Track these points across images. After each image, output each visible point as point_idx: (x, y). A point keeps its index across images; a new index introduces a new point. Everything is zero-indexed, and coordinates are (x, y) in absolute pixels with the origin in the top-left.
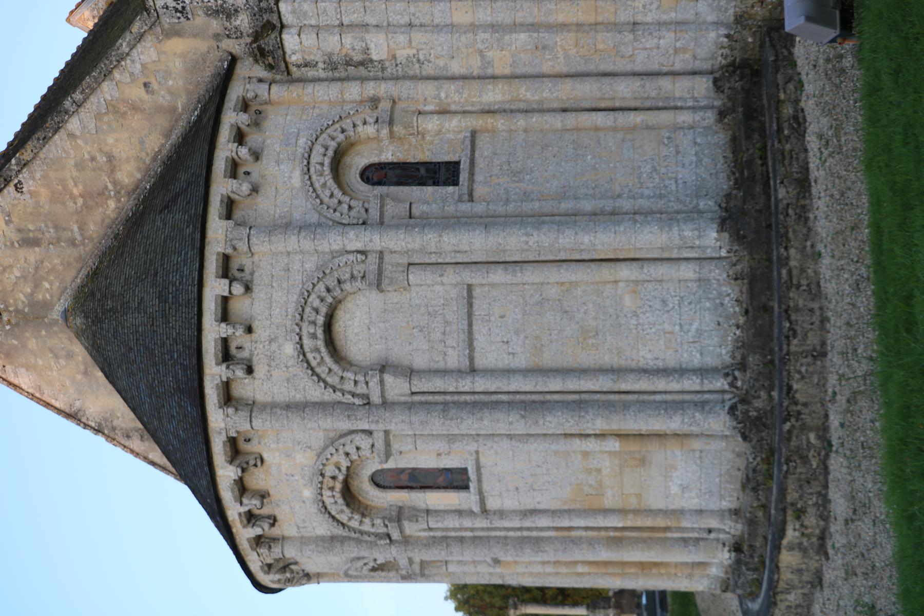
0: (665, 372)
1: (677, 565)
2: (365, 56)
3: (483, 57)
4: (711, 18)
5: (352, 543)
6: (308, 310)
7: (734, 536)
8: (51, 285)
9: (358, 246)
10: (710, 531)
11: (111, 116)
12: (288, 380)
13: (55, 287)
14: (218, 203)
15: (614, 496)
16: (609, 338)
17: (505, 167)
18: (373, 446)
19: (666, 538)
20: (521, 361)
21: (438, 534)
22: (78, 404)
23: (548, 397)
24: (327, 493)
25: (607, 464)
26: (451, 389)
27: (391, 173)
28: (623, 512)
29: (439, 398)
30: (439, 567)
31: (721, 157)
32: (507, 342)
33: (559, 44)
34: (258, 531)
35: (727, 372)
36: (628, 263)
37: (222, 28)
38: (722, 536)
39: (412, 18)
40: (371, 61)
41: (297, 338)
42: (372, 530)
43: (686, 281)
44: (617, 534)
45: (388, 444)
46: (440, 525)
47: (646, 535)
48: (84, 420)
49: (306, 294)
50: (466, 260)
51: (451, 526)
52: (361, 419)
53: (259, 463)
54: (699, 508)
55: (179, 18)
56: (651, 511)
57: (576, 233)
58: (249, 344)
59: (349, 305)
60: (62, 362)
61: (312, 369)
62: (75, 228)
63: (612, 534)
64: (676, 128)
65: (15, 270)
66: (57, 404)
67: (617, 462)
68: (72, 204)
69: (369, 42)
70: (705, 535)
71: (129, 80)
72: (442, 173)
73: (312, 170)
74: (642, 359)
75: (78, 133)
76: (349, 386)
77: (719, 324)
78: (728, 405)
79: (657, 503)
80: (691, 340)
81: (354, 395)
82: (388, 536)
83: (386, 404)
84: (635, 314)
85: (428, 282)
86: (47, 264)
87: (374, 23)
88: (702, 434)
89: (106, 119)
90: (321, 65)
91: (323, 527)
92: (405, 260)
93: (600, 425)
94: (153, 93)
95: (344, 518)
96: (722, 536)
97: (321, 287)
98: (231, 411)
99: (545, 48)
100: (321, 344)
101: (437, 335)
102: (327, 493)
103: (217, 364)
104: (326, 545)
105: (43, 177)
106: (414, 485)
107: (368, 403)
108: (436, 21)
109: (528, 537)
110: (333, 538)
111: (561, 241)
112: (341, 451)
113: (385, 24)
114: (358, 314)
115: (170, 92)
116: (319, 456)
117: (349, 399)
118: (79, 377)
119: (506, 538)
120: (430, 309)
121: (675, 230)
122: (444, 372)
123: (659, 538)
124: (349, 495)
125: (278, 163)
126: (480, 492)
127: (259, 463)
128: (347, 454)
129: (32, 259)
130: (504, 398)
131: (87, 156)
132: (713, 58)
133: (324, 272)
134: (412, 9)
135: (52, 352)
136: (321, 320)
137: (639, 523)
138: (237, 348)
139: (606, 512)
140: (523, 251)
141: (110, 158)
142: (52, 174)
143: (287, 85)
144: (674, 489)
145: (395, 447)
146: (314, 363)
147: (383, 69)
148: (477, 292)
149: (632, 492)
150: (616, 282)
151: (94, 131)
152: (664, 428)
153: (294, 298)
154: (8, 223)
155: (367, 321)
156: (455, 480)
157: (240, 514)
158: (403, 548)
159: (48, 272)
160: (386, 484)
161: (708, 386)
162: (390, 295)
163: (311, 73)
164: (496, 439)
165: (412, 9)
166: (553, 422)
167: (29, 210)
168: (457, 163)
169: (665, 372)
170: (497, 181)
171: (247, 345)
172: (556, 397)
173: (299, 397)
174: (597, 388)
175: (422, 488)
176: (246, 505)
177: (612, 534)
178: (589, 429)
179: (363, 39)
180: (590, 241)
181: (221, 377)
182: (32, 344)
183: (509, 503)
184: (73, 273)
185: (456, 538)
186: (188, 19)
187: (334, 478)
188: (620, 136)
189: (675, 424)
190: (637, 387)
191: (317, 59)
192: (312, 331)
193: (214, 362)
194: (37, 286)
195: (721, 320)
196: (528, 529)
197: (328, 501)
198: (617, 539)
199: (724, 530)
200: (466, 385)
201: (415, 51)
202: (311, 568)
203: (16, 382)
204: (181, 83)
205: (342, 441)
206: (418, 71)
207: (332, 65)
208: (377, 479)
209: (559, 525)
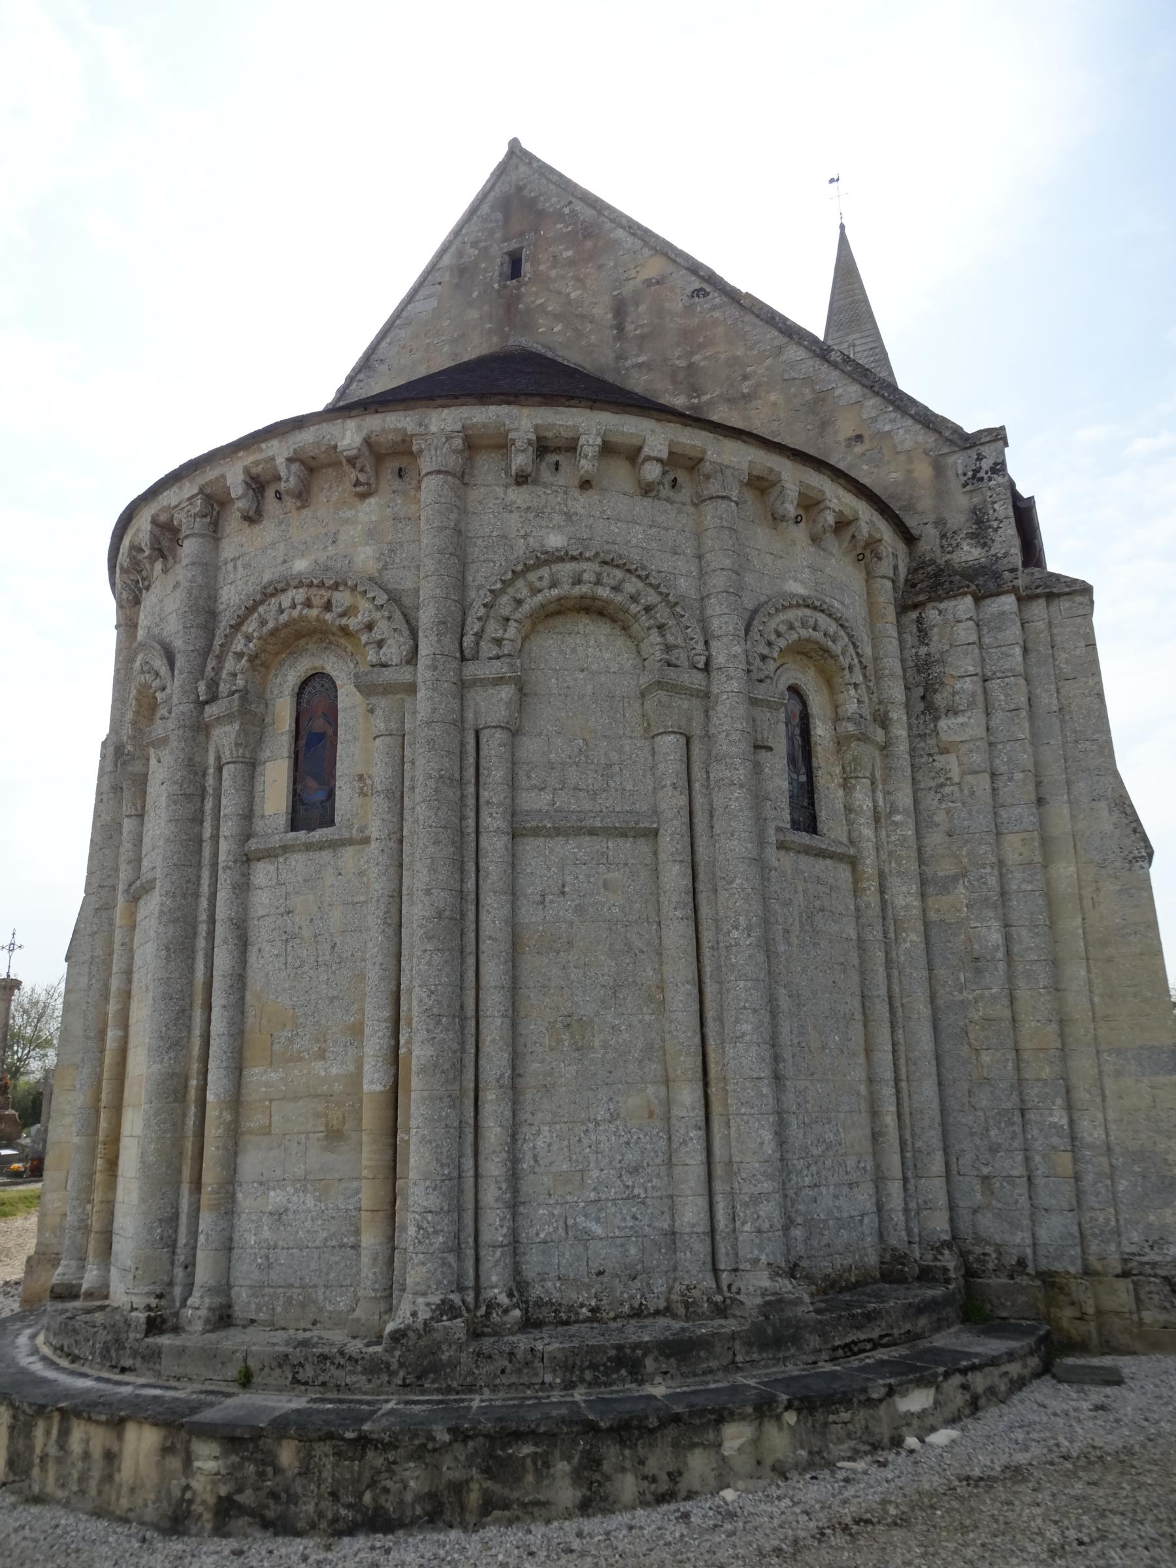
0: (514, 1177)
1: (109, 1206)
2: (944, 711)
3: (955, 879)
4: (1043, 1234)
6: (619, 574)
7: (176, 1314)
8: (559, 333)
9: (720, 659)
12: (504, 537)
14: (769, 464)
15: (268, 1084)
19: (179, 1183)
20: (529, 915)
21: (210, 781)
23: (471, 960)
24: (300, 595)
25: (334, 1071)
26: (485, 795)
28: (236, 1100)
29: (471, 772)
30: (135, 805)
31: (850, 1261)
32: (563, 893)
33: (987, 992)
37: (955, 528)
38: (178, 1291)
39: (1005, 777)
40: (936, 719)
41: (575, 553)
42: (224, 675)
43: (672, 1208)
44: (192, 1094)
45: (387, 690)
46: (226, 783)
47: (189, 1146)
48: (361, 376)
49: (644, 573)
51: (224, 802)
52: (439, 641)
53: (360, 489)
54: (235, 1245)
55: (965, 474)
56: (236, 1154)
57: (755, 1011)
59: (621, 642)
60: (446, 349)
61: (523, 573)
62: (641, 360)
63: (194, 1083)
64: (879, 1180)
65: (579, 292)
66: (384, 344)
67: (337, 1088)
68: (677, 354)
69: (968, 714)
70: (181, 1258)
71: (865, 416)
73: (808, 612)
74: (534, 1129)
75: (783, 358)
76: (493, 629)
77: (600, 1273)
78: (456, 1298)
79: (251, 1163)
80: (570, 1222)
81: (479, 636)
82: (213, 698)
83: (463, 686)
84: (613, 1117)
85: (661, 767)
86: (589, 327)
87: (992, 724)
88: (394, 1249)
90: (923, 650)
91: (231, 596)
93: (419, 1051)
94: (849, 446)
95: (251, 626)
96: (178, 1291)
97: (652, 598)
98: (458, 442)
99: (978, 972)
100: (565, 589)
102: (300, 595)
103: (536, 427)
104: (201, 602)
106: (302, 742)
107: (463, 659)
109: (195, 934)
110: (212, 615)
111: (742, 984)
112: (377, 615)
113: (992, 739)
114: (607, 656)
116: (370, 579)
117: (473, 627)
119: (197, 895)
120: (616, 768)
121: (767, 1186)
122: (513, 784)
123: (179, 1171)
124: (292, 638)
125: (813, 569)
126: (286, 849)
127: (360, 489)
128: (370, 627)
129: (597, 311)
130: (470, 885)
132: (978, 1240)
133: (677, 603)
134: (1019, 776)
136: (604, 592)
137: (212, 1131)
138: (557, 464)
139: (237, 1069)
141: (747, 398)
142: (720, 330)
144: (275, 1198)
145: (383, 703)
146: (532, 577)
147: (922, 736)
148: (643, 846)
149: (275, 1118)
150: (667, 1082)
151: (786, 376)
152: (413, 1175)
153: (635, 555)
155: (594, 667)
156: (311, 808)
157: (272, 459)
158: (188, 723)
159: (575, 330)
160: (306, 696)
161: (490, 1258)
162: (637, 705)
164: (392, 870)
165: (1019, 776)
166: (422, 967)
169: (514, 1177)
170: (800, 889)
171: (560, 480)
172: (471, 974)
173: (475, 552)
174: (487, 1048)
175: (296, 753)
176: (288, 468)
177: (194, 1083)
179: (971, 705)
180: (743, 1035)
181: (517, 430)
182: (473, 314)
183: (262, 901)
185: (202, 812)
186: (965, 485)
187: (328, 606)
188: (863, 1089)
189: (419, 1195)
191: (932, 644)
192: (586, 577)
193: (540, 422)
194: (557, 317)
195: (605, 1279)
196: (211, 934)
197: (286, 600)
199: (190, 1295)
200: (494, 820)
201: (956, 779)
205: (398, 615)
206: (922, 785)
208: (316, 683)
209: (216, 985)
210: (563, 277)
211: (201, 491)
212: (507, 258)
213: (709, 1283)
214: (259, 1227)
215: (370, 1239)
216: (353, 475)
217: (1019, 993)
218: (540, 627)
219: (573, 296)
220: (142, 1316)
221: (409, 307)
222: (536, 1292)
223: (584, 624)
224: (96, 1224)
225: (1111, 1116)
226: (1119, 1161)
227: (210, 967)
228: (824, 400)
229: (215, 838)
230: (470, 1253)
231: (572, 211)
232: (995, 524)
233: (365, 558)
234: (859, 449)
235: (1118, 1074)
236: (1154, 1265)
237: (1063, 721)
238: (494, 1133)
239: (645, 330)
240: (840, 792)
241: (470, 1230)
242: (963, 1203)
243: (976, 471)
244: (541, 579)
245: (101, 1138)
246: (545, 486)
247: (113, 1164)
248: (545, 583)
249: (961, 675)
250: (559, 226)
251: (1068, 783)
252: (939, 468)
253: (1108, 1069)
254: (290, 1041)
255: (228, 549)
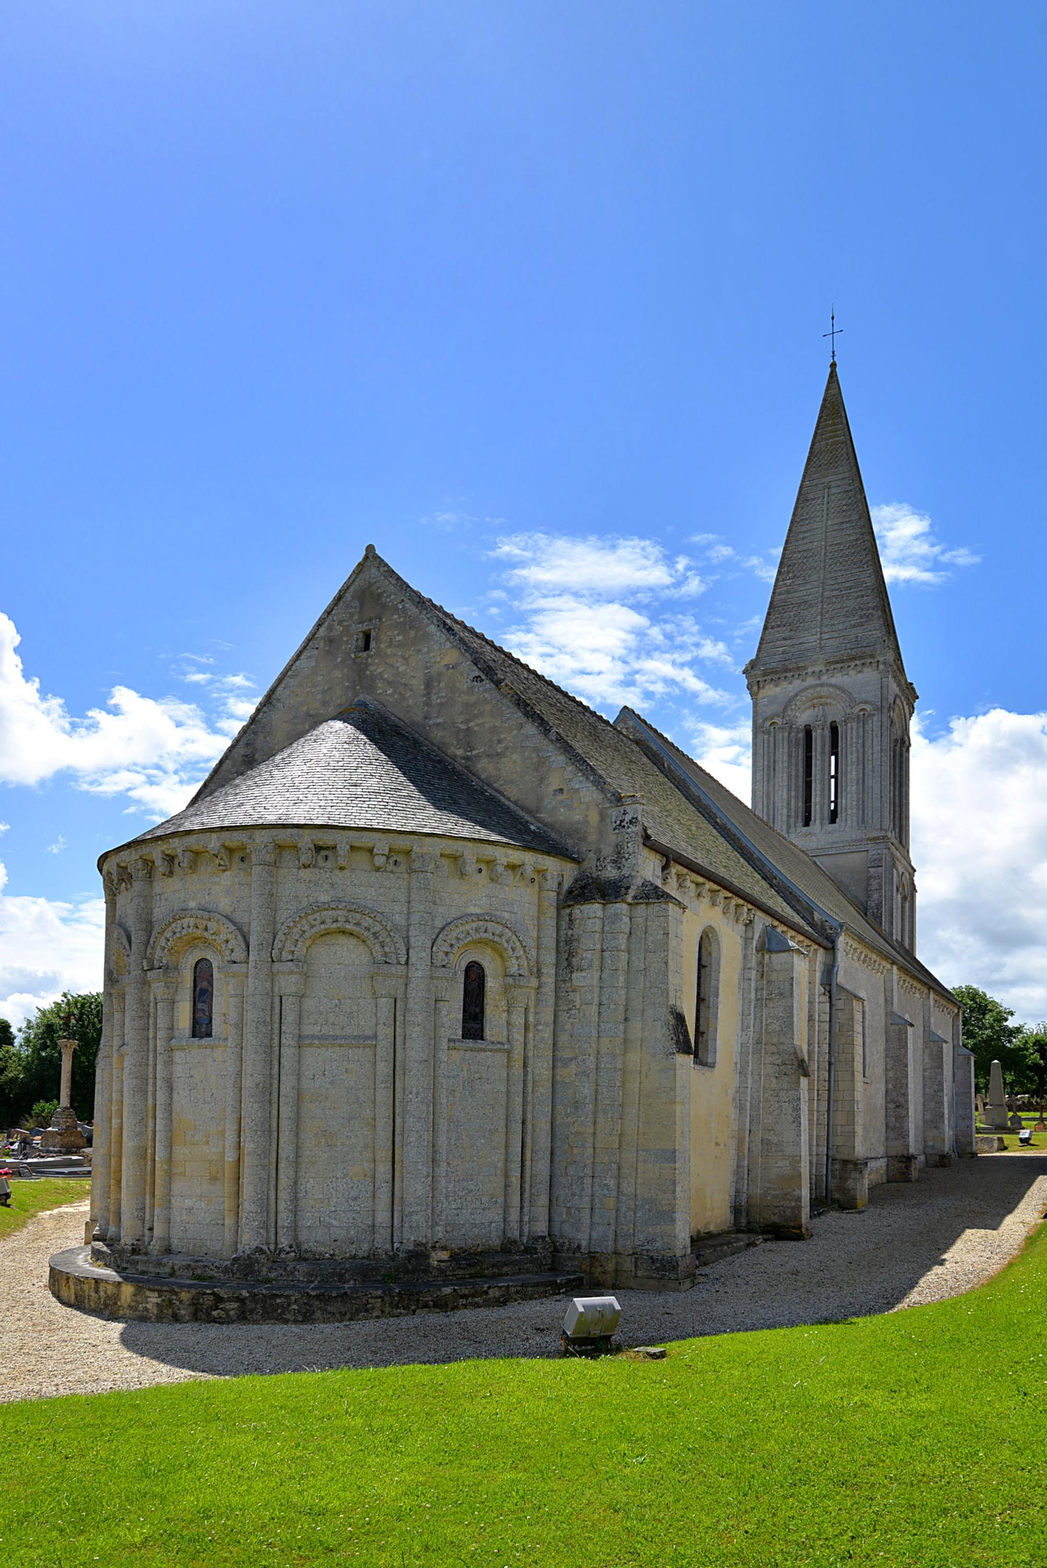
0: (295, 1199)
3: (571, 1059)
5: (145, 938)
6: (358, 916)
10: (151, 1229)
11: (535, 760)
13: (388, 698)
16: (326, 1155)
17: (477, 1076)
18: (235, 962)
20: (306, 1084)
22: (280, 705)
23: (275, 1106)
27: (475, 985)
28: (169, 1160)
34: (158, 862)
35: (296, 1245)
36: (391, 1171)
40: (572, 972)
43: (373, 1215)
47: (148, 1178)
48: (265, 709)
50: (397, 1044)
58: (330, 866)
59: (362, 948)
60: (319, 697)
62: (439, 721)
64: (506, 1207)
65: (405, 667)
66: (280, 688)
72: (473, 1023)
78: (265, 1247)
79: (177, 1186)
81: (281, 950)
84: (345, 1176)
86: (409, 694)
89: (534, 755)
90: (570, 932)
92: (399, 996)
93: (248, 1146)
94: (554, 795)
96: (146, 1239)
98: (271, 847)
99: (576, 1108)
101: (332, 1018)
105: (485, 699)
108: (602, 1025)
112: (229, 936)
115: (554, 809)
117: (278, 944)
118: (305, 709)
122: (300, 1023)
129: (414, 682)
130: (275, 1070)
131: (502, 736)
132: (562, 1236)
135: (329, 689)
136: (349, 927)
139: (170, 1147)
140: (404, 1089)
141: (500, 755)
142: (488, 707)
143: (555, 904)
144: (188, 1203)
147: (564, 981)
154: (447, 666)
156: (201, 1028)
159: (400, 694)
163: (564, 924)
166: (251, 1109)
167: (457, 684)
168: (482, 1038)
169: (295, 1199)
171: (329, 864)
172: (275, 1112)
175: (194, 998)
177: (149, 1151)
178: (246, 1137)
182: (337, 674)
183: (179, 1070)
184: (401, 715)
187: (206, 929)
188: (500, 1165)
190: (282, 1176)
194: (390, 683)
195: (338, 1243)
196: (155, 1083)
198: (144, 1155)
200: (288, 1041)
202: (121, 900)
203: (302, 657)
204: (562, 818)
207: (569, 941)
210: (395, 655)
211: (141, 858)
212: (361, 635)
213: (388, 1246)
214: (181, 1215)
215: (229, 1221)
216: (217, 861)
217: (598, 1120)
218: (317, 941)
219: (400, 669)
220: (130, 1248)
221: (297, 663)
222: (305, 1247)
223: (342, 939)
224: (112, 1208)
225: (639, 1181)
226: (639, 1203)
227: (155, 1100)
228: (544, 763)
229: (155, 1038)
230: (273, 1230)
231: (404, 607)
232: (627, 856)
233: (225, 904)
234: (560, 797)
235: (645, 1161)
236: (648, 1251)
237: (645, 976)
238: (284, 1181)
239: (443, 700)
240: (505, 1015)
241: (273, 1219)
242: (556, 1218)
243: (622, 821)
244: (315, 920)
245: (112, 1169)
246: (320, 868)
247: (119, 1182)
248: (318, 922)
249: (588, 947)
250: (396, 617)
251: (643, 1011)
252: (603, 816)
253: (641, 1158)
254: (193, 1136)
255: (157, 889)
